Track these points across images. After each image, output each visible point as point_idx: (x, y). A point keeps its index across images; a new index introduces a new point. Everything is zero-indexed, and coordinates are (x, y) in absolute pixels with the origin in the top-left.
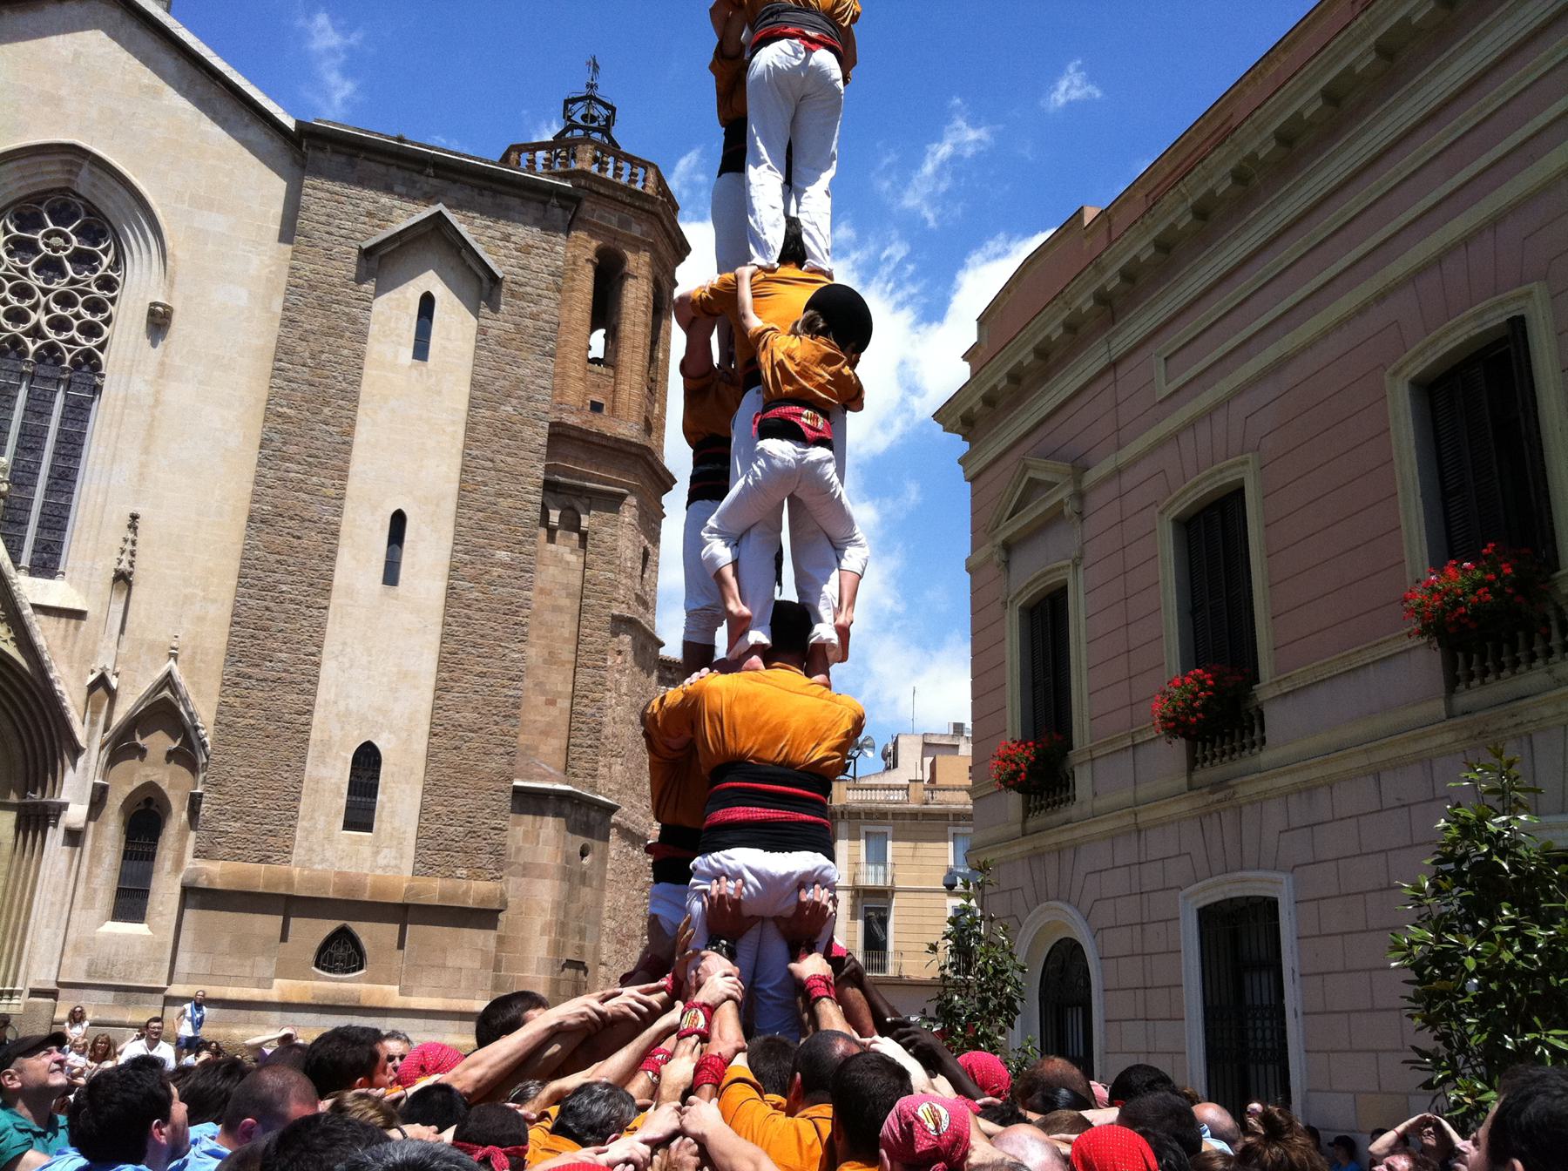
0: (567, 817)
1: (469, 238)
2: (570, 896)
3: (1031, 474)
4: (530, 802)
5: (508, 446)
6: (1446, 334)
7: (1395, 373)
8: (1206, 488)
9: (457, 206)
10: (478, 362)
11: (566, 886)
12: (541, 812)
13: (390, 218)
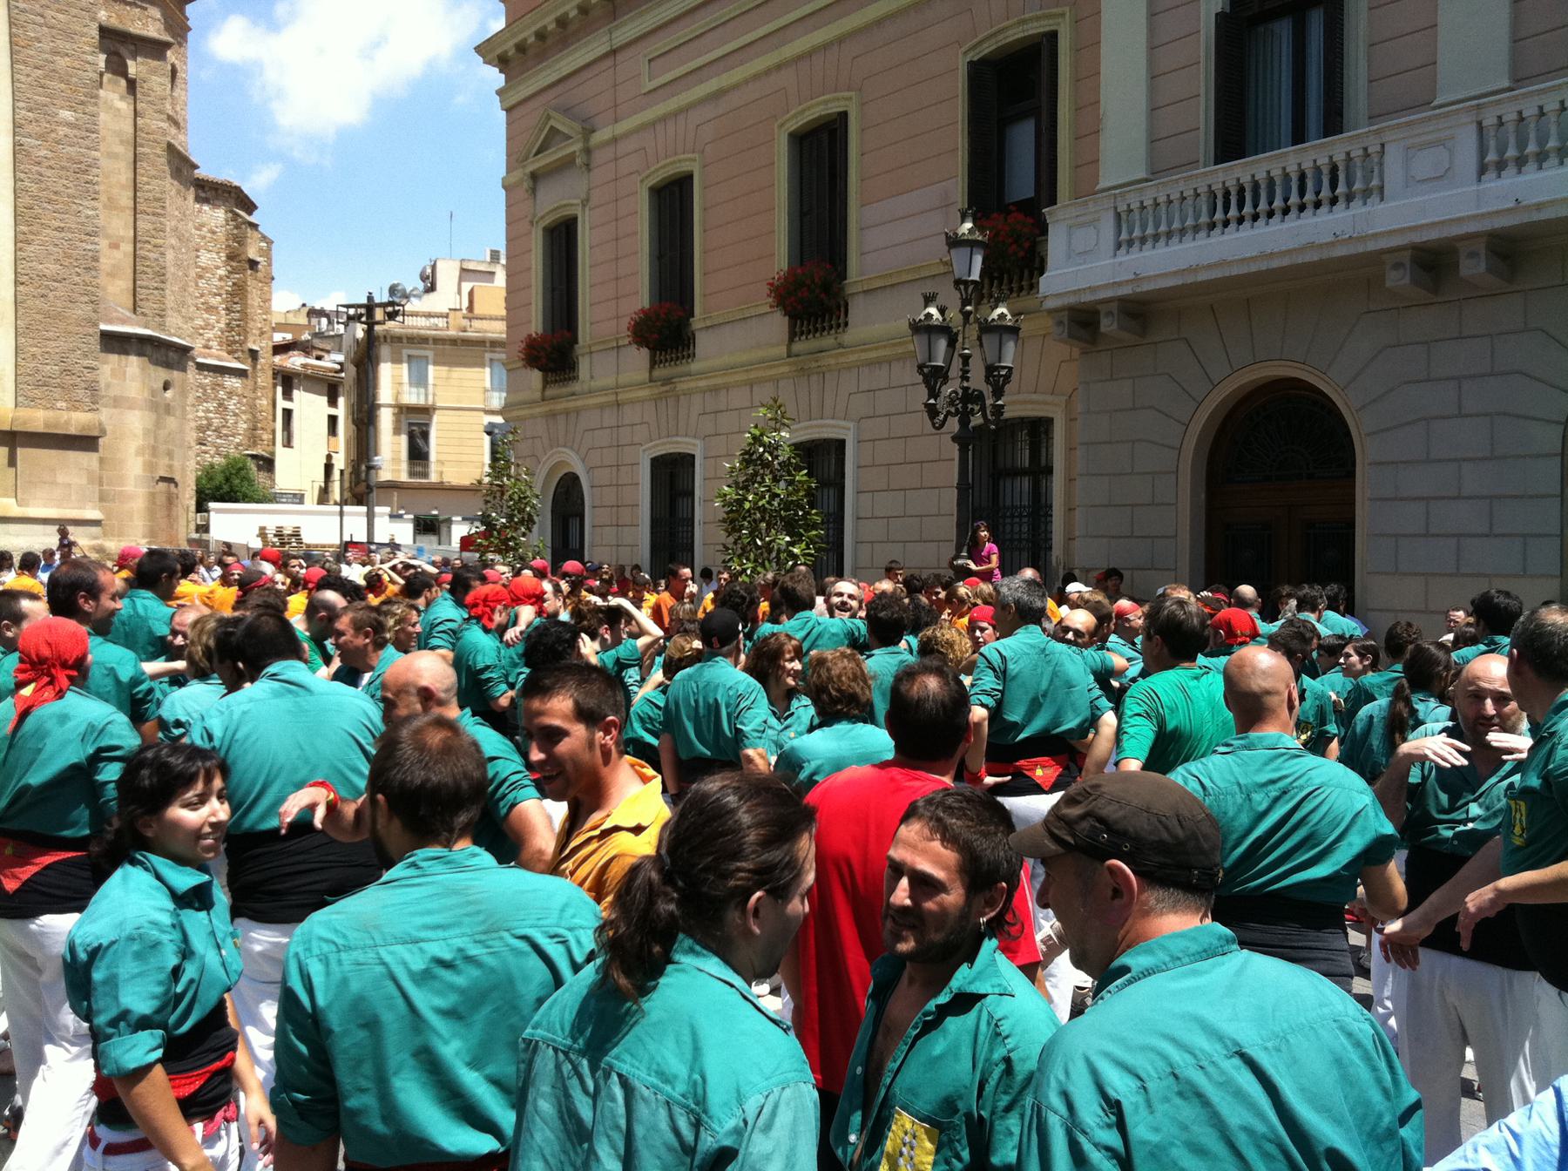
2: (158, 424)
3: (552, 123)
4: (115, 343)
6: (809, 108)
11: (154, 416)
12: (126, 353)
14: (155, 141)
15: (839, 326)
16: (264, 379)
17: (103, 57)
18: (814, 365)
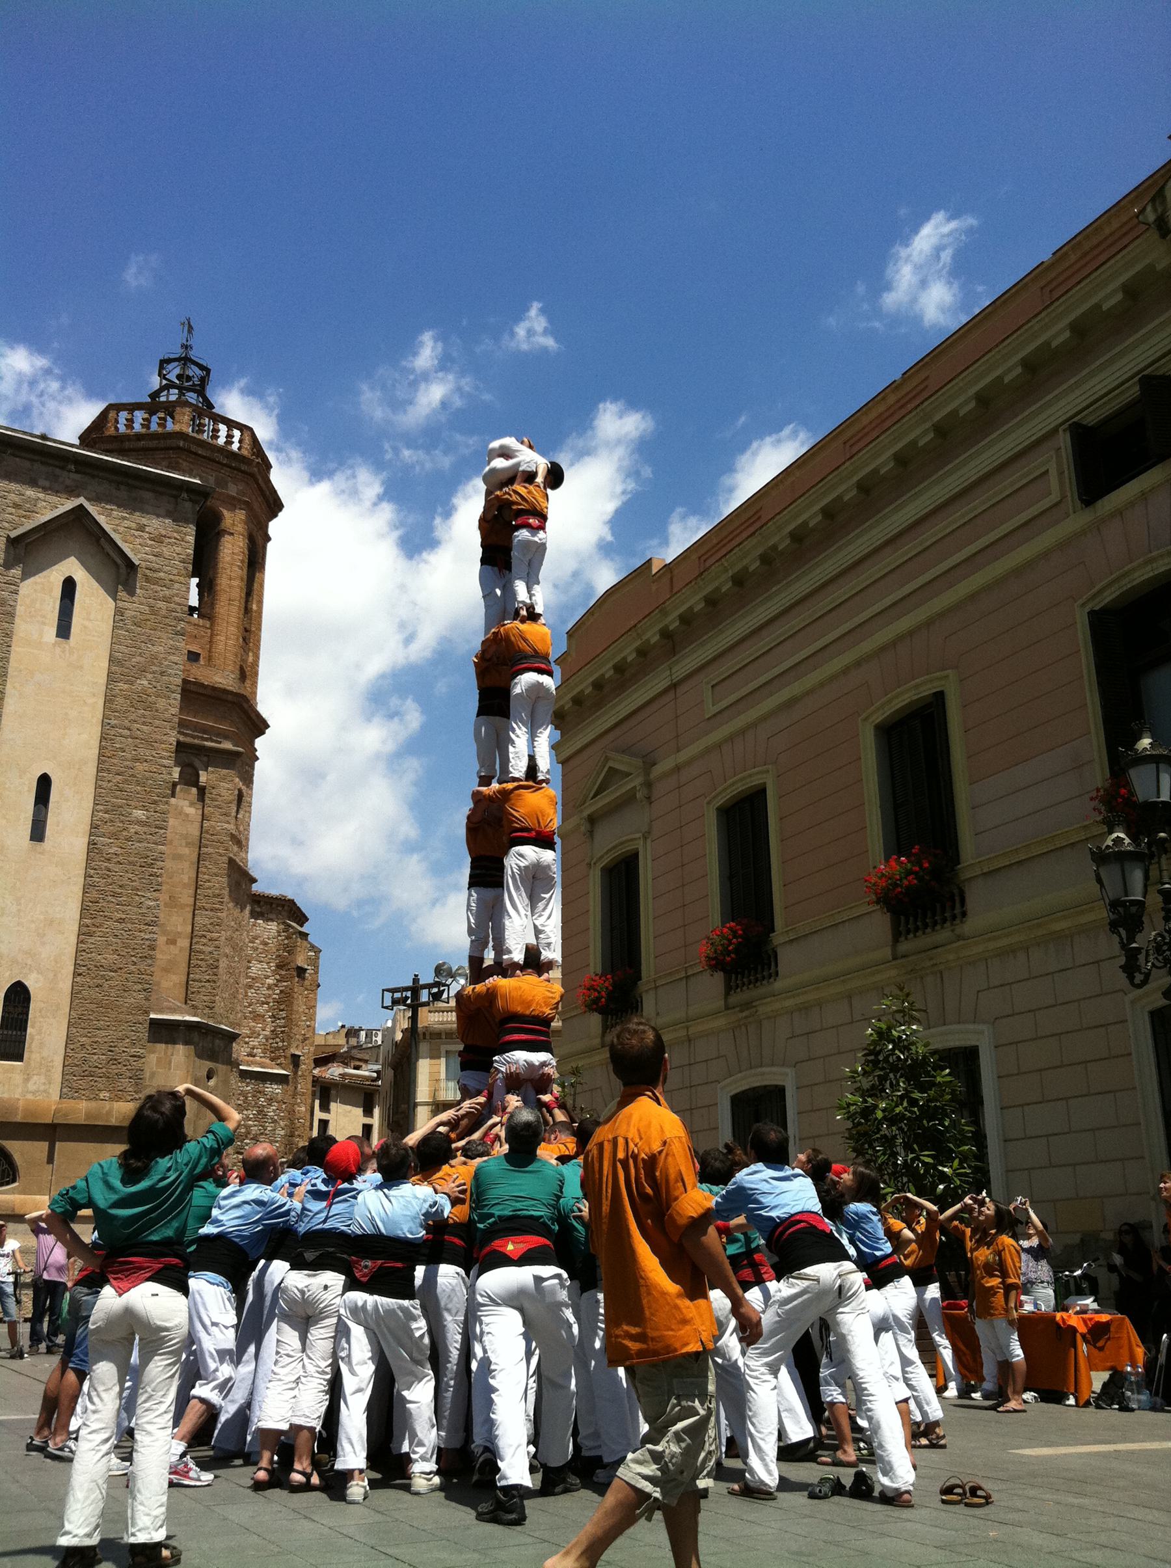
0: (196, 1045)
1: (107, 528)
3: (610, 764)
4: (164, 1032)
5: (144, 716)
6: (897, 697)
7: (866, 719)
8: (740, 787)
9: (96, 499)
10: (115, 640)
12: (173, 1041)
13: (35, 509)
14: (219, 841)
15: (954, 918)
16: (304, 1086)
17: (178, 769)
18: (929, 963)
